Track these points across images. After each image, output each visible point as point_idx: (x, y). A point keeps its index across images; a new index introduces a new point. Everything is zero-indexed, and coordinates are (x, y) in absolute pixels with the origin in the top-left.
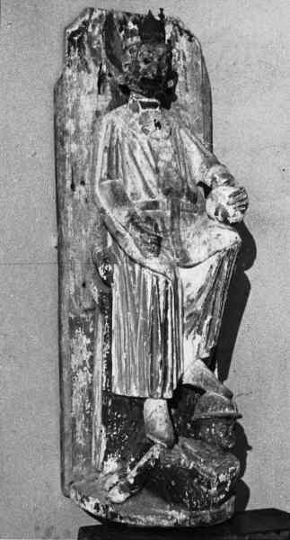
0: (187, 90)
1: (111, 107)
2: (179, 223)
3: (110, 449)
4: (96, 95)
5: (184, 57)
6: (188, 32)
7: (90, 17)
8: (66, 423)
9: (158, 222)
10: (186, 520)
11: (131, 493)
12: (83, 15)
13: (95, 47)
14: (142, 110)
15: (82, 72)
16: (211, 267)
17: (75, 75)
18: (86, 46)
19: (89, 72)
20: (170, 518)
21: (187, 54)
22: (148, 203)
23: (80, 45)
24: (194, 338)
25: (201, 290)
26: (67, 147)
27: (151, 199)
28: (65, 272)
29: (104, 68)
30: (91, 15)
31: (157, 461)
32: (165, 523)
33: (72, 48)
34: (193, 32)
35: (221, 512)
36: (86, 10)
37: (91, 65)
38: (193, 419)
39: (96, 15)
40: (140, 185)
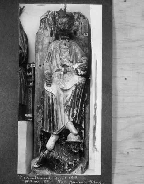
1: (54, 40)
3: (42, 149)
5: (81, 23)
7: (49, 13)
8: (35, 139)
11: (41, 165)
13: (50, 22)
14: (61, 40)
15: (45, 30)
19: (47, 30)
21: (82, 22)
25: (70, 98)
29: (53, 29)
31: (46, 155)
33: (42, 23)
36: (47, 11)
37: (48, 28)
38: (67, 141)
39: (50, 13)
40: (56, 65)
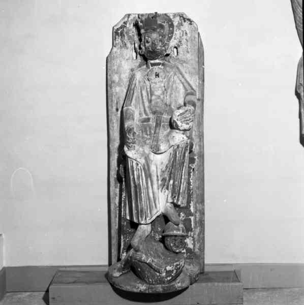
0: (188, 52)
2: (159, 130)
4: (131, 60)
5: (186, 33)
6: (189, 20)
7: (128, 19)
9: (148, 129)
10: (146, 290)
12: (124, 18)
13: (130, 35)
16: (171, 154)
17: (119, 51)
18: (125, 35)
20: (137, 287)
21: (188, 32)
22: (145, 118)
23: (122, 35)
24: (165, 192)
26: (113, 89)
27: (147, 117)
28: (113, 154)
30: (128, 18)
31: (131, 257)
32: (135, 290)
33: (117, 37)
34: (192, 19)
35: (170, 286)
36: (126, 15)
